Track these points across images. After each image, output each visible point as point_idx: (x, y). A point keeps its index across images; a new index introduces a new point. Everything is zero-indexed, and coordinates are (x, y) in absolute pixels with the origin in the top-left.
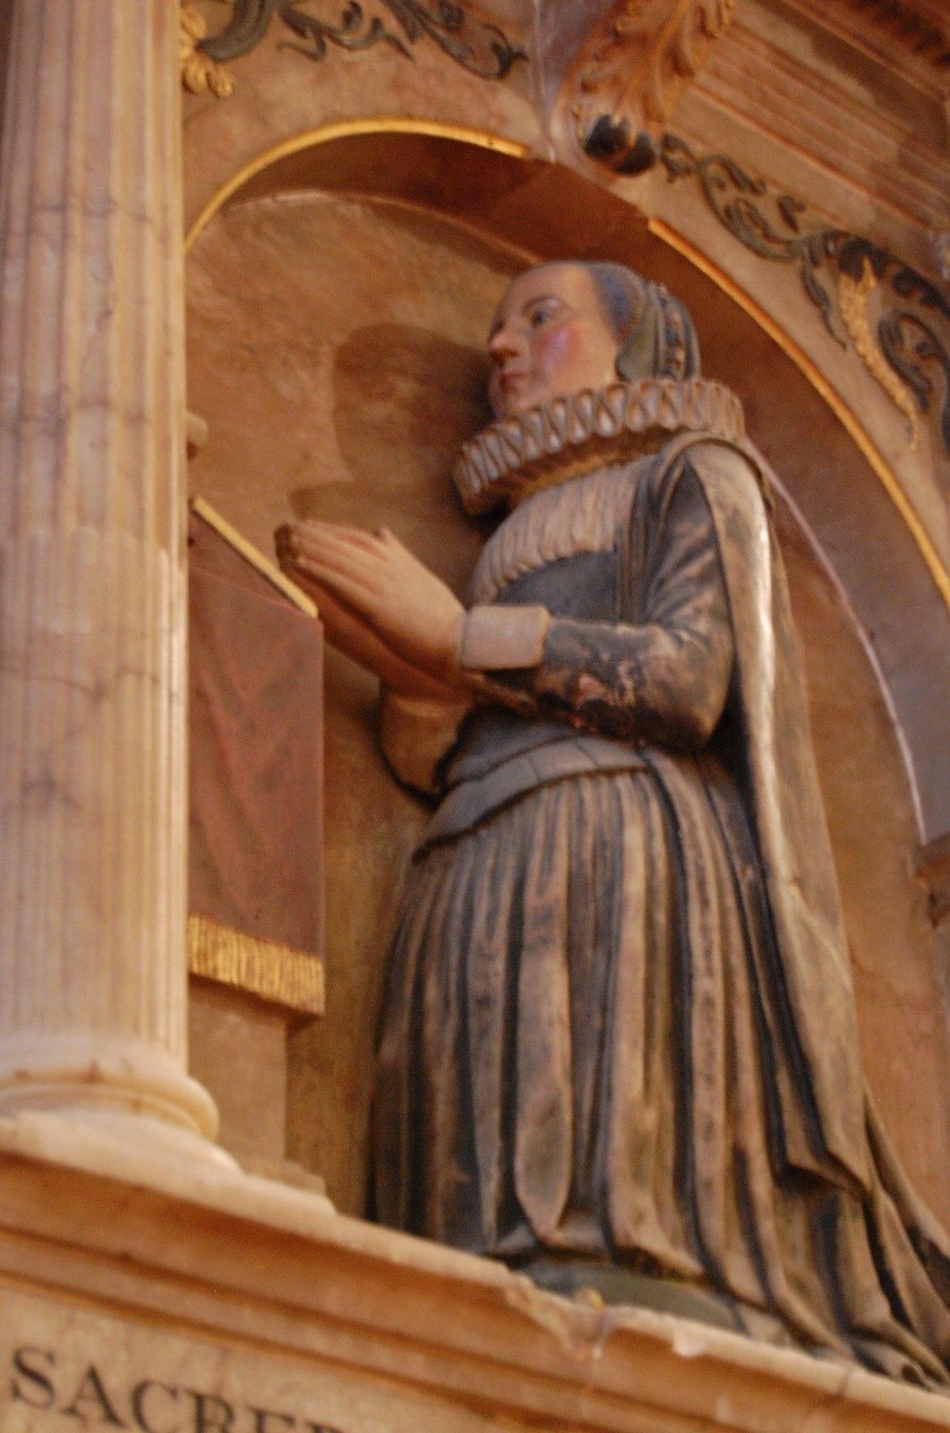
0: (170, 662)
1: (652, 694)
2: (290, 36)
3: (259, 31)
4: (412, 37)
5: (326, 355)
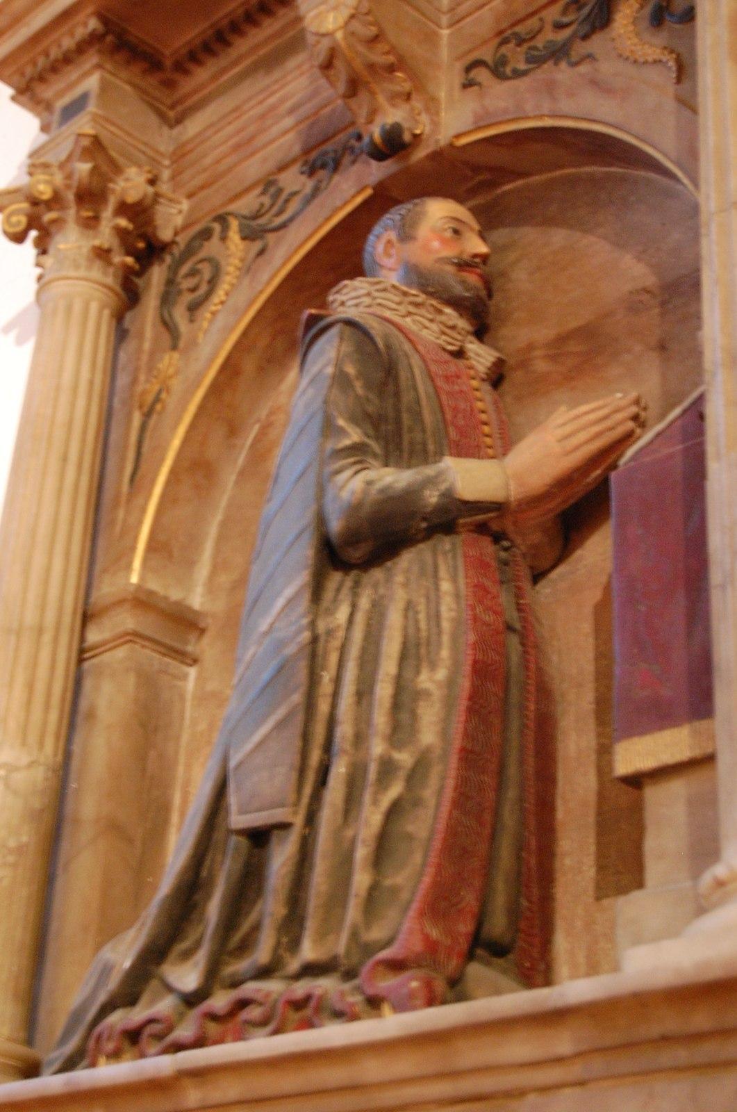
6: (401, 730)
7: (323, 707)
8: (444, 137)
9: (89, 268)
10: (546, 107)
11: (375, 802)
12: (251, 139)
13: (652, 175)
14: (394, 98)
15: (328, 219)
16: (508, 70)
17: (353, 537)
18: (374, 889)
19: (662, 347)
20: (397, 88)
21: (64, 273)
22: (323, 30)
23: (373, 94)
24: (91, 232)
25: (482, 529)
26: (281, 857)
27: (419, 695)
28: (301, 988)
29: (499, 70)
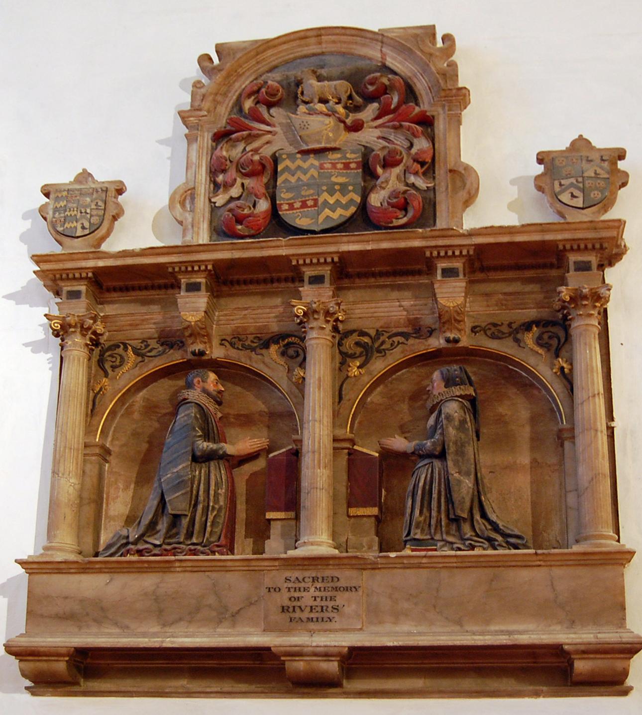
0: (600, 411)
1: (428, 452)
2: (378, 355)
3: (371, 357)
4: (407, 340)
5: (407, 400)
6: (216, 501)
7: (194, 492)
8: (214, 356)
9: (84, 349)
10: (248, 362)
11: (211, 514)
12: (137, 325)
13: (276, 390)
14: (201, 342)
15: (169, 362)
16: (236, 347)
17: (202, 457)
18: (211, 531)
19: (268, 427)
20: (204, 340)
21: (77, 348)
22: (188, 320)
23: (196, 339)
24: (253, 428)
25: (227, 460)
26: (185, 522)
27: (218, 494)
28: (192, 547)
29: (232, 345)
